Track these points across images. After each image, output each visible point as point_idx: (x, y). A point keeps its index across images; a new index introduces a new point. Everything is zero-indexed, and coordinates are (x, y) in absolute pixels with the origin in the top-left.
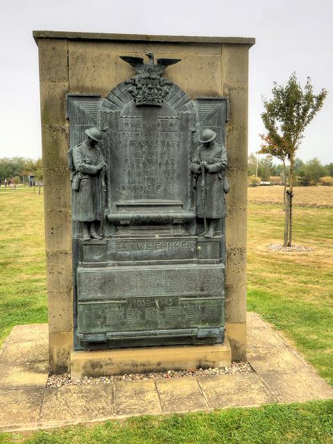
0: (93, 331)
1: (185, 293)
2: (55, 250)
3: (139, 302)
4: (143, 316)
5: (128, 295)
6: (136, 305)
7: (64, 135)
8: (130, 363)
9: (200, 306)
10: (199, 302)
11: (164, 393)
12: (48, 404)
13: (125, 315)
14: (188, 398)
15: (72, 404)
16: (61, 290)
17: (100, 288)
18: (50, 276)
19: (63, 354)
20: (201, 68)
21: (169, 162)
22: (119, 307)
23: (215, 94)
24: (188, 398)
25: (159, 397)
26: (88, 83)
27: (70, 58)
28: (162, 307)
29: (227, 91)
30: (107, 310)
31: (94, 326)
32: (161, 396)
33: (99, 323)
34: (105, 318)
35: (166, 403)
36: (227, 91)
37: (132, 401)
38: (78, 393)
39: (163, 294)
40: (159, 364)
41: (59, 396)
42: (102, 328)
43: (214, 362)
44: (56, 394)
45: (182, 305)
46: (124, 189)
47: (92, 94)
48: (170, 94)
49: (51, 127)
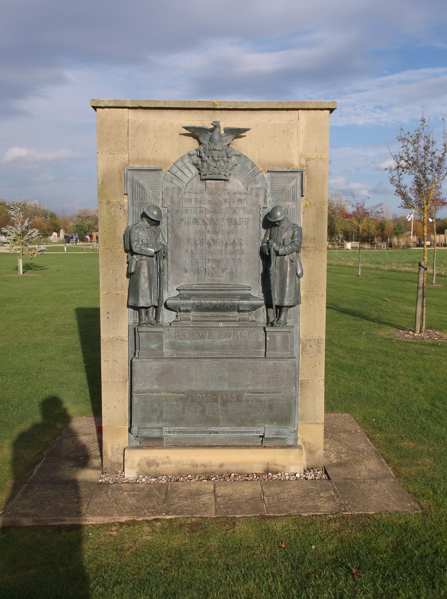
0: (148, 425)
1: (251, 388)
2: (111, 336)
3: (199, 397)
4: (203, 412)
5: (186, 388)
6: (196, 399)
7: (122, 212)
8: (190, 463)
9: (267, 403)
10: (266, 398)
11: (222, 496)
12: (97, 500)
13: (183, 409)
14: (246, 502)
15: (121, 502)
16: (116, 380)
17: (157, 379)
18: (376, 231)
19: (118, 450)
20: (275, 136)
21: (237, 242)
22: (177, 401)
23: (290, 165)
24: (246, 502)
25: (216, 499)
26: (149, 155)
27: (130, 128)
28: (224, 403)
29: (303, 162)
30: (164, 403)
31: (150, 421)
32: (218, 499)
33: (155, 417)
34: (162, 412)
35: (222, 506)
36: (303, 162)
37: (185, 503)
38: (129, 491)
39: (225, 387)
40: (221, 465)
41: (109, 493)
42: (158, 422)
43: (284, 467)
44: (106, 492)
45: (247, 401)
46: (186, 271)
47: (152, 166)
48: (239, 166)
49: (108, 202)
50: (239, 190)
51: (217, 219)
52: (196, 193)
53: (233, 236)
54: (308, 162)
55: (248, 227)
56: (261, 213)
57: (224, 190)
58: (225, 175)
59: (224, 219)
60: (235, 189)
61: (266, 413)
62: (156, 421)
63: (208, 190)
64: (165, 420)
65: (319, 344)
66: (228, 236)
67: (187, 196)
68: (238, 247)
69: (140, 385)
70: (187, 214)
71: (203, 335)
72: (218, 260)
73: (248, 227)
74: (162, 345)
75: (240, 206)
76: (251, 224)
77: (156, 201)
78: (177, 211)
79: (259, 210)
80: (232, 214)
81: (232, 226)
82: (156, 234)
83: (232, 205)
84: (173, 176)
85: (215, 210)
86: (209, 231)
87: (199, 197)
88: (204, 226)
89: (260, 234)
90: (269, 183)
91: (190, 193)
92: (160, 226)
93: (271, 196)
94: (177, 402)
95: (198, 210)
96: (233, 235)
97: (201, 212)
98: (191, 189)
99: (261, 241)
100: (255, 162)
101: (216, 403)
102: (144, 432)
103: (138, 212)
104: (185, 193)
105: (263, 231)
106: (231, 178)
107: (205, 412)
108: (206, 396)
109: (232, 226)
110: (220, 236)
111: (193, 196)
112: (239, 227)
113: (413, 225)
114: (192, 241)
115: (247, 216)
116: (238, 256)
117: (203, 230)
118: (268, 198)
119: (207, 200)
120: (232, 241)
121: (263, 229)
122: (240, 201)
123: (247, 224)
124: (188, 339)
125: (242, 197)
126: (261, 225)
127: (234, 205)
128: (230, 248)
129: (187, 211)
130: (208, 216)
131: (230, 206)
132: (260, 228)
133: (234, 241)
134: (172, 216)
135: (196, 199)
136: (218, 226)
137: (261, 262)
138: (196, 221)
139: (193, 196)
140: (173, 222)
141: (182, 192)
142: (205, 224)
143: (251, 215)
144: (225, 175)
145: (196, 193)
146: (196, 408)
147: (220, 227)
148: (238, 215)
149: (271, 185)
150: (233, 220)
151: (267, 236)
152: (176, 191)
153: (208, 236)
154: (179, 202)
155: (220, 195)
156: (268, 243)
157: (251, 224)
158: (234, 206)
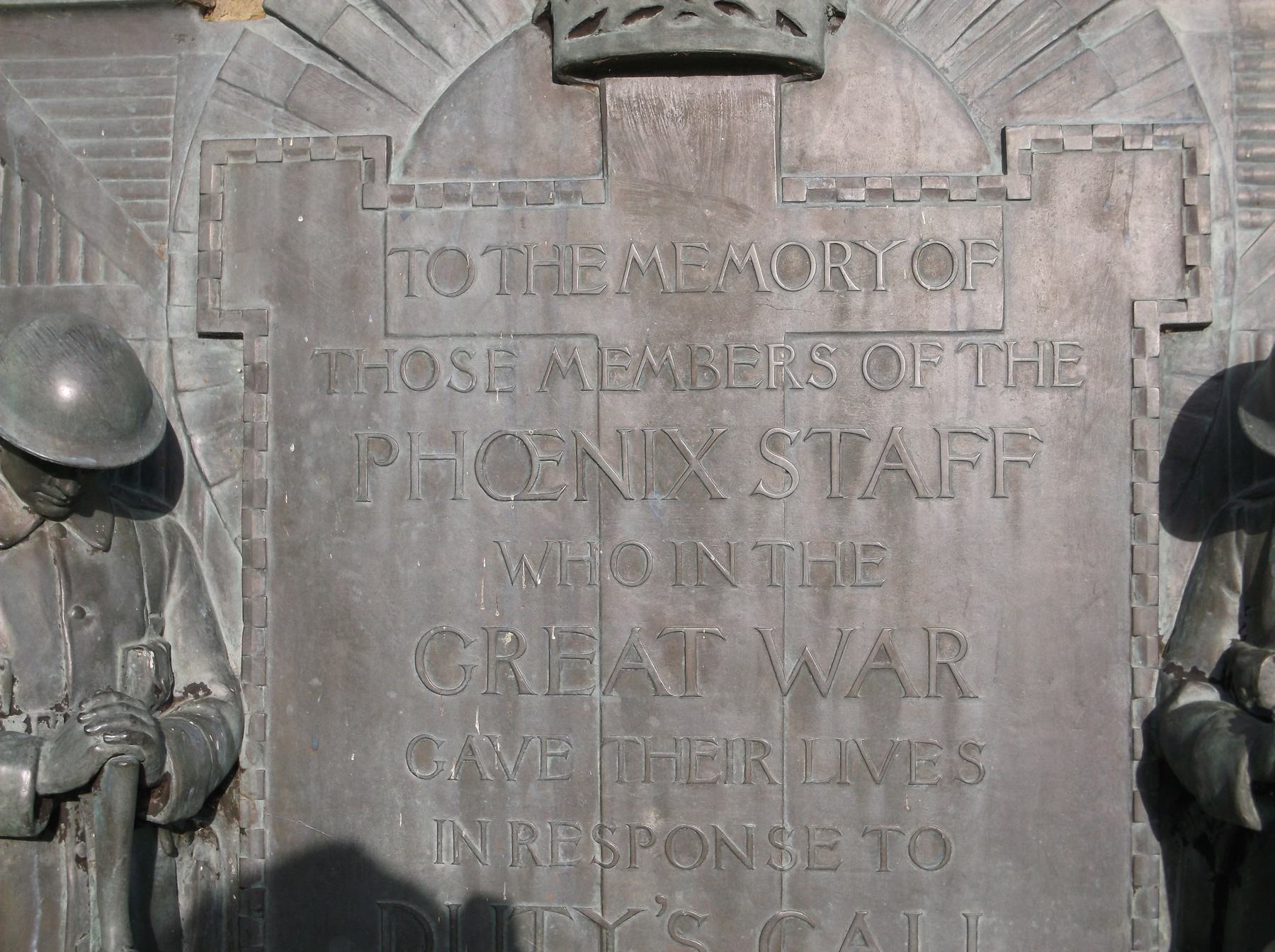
21: (911, 659)
50: (928, 158)
51: (712, 446)
52: (513, 198)
53: (868, 610)
55: (1016, 512)
56: (1146, 373)
57: (780, 161)
58: (783, 19)
59: (775, 441)
60: (888, 156)
63: (629, 164)
66: (825, 607)
67: (424, 231)
68: (917, 719)
70: (423, 403)
72: (720, 842)
73: (1016, 512)
75: (938, 311)
76: (1045, 484)
77: (149, 280)
78: (333, 372)
79: (1126, 347)
80: (857, 387)
81: (862, 512)
82: (96, 595)
83: (857, 301)
84: (304, 55)
85: (691, 356)
86: (630, 562)
87: (539, 228)
88: (581, 512)
89: (1142, 587)
90: (1218, 89)
91: (452, 195)
92: (180, 517)
95: (532, 352)
96: (869, 602)
97: (551, 372)
98: (466, 167)
99: (1155, 658)
104: (403, 196)
105: (1174, 560)
106: (841, 53)
109: (862, 512)
110: (744, 608)
111: (486, 224)
112: (931, 517)
114: (472, 656)
115: (1007, 409)
116: (924, 804)
117: (584, 547)
118: (1218, 230)
119: (611, 262)
120: (859, 654)
121: (1166, 539)
122: (936, 262)
123: (1005, 485)
125: (958, 225)
126: (1150, 493)
127: (879, 304)
128: (843, 720)
129: (423, 365)
130: (629, 412)
131: (843, 312)
132: (1140, 531)
133: (884, 652)
134: (287, 424)
135: (509, 255)
136: (721, 514)
137: (1154, 859)
138: (507, 463)
139: (486, 224)
140: (289, 469)
141: (381, 193)
142: (604, 495)
143: (1046, 403)
144: (783, 19)
145: (513, 198)
147: (738, 519)
148: (913, 398)
149: (1242, 111)
150: (871, 455)
151: (1218, 606)
152: (324, 178)
153: (631, 605)
154: (352, 284)
155: (741, 211)
156: (1232, 676)
157: (1045, 484)
158: (880, 311)
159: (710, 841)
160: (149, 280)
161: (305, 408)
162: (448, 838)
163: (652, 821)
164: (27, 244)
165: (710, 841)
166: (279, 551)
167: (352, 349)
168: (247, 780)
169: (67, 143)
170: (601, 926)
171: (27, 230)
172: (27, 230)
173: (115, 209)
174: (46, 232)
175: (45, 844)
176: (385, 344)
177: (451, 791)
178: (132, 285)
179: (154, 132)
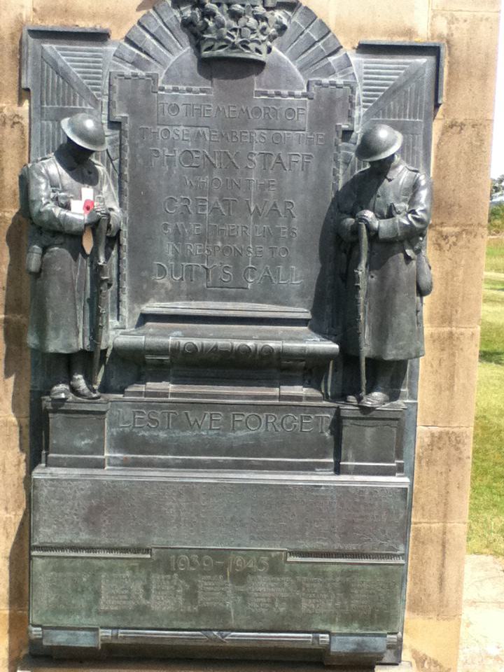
0: (66, 622)
9: (338, 579)
21: (280, 208)
31: (69, 612)
54: (453, 27)
61: (335, 601)
62: (84, 613)
64: (106, 613)
65: (460, 446)
69: (48, 531)
71: (196, 421)
74: (101, 441)
93: (362, 104)
94: (134, 572)
100: (331, 25)
101: (221, 577)
102: (57, 635)
103: (53, 133)
107: (196, 595)
108: (200, 560)
113: (373, 462)
124: (162, 429)
146: (176, 587)
159: (233, 249)
160: (96, 107)
161: (138, 141)
162: (171, 247)
163: (219, 244)
164: (64, 95)
165: (233, 249)
166: (130, 177)
167: (149, 128)
168: (122, 234)
169: (74, 70)
170: (206, 269)
171: (64, 90)
172: (64, 90)
173: (87, 88)
174: (69, 94)
175: (269, 20)
176: (158, 127)
177: (172, 236)
178: (92, 108)
179: (409, 115)
